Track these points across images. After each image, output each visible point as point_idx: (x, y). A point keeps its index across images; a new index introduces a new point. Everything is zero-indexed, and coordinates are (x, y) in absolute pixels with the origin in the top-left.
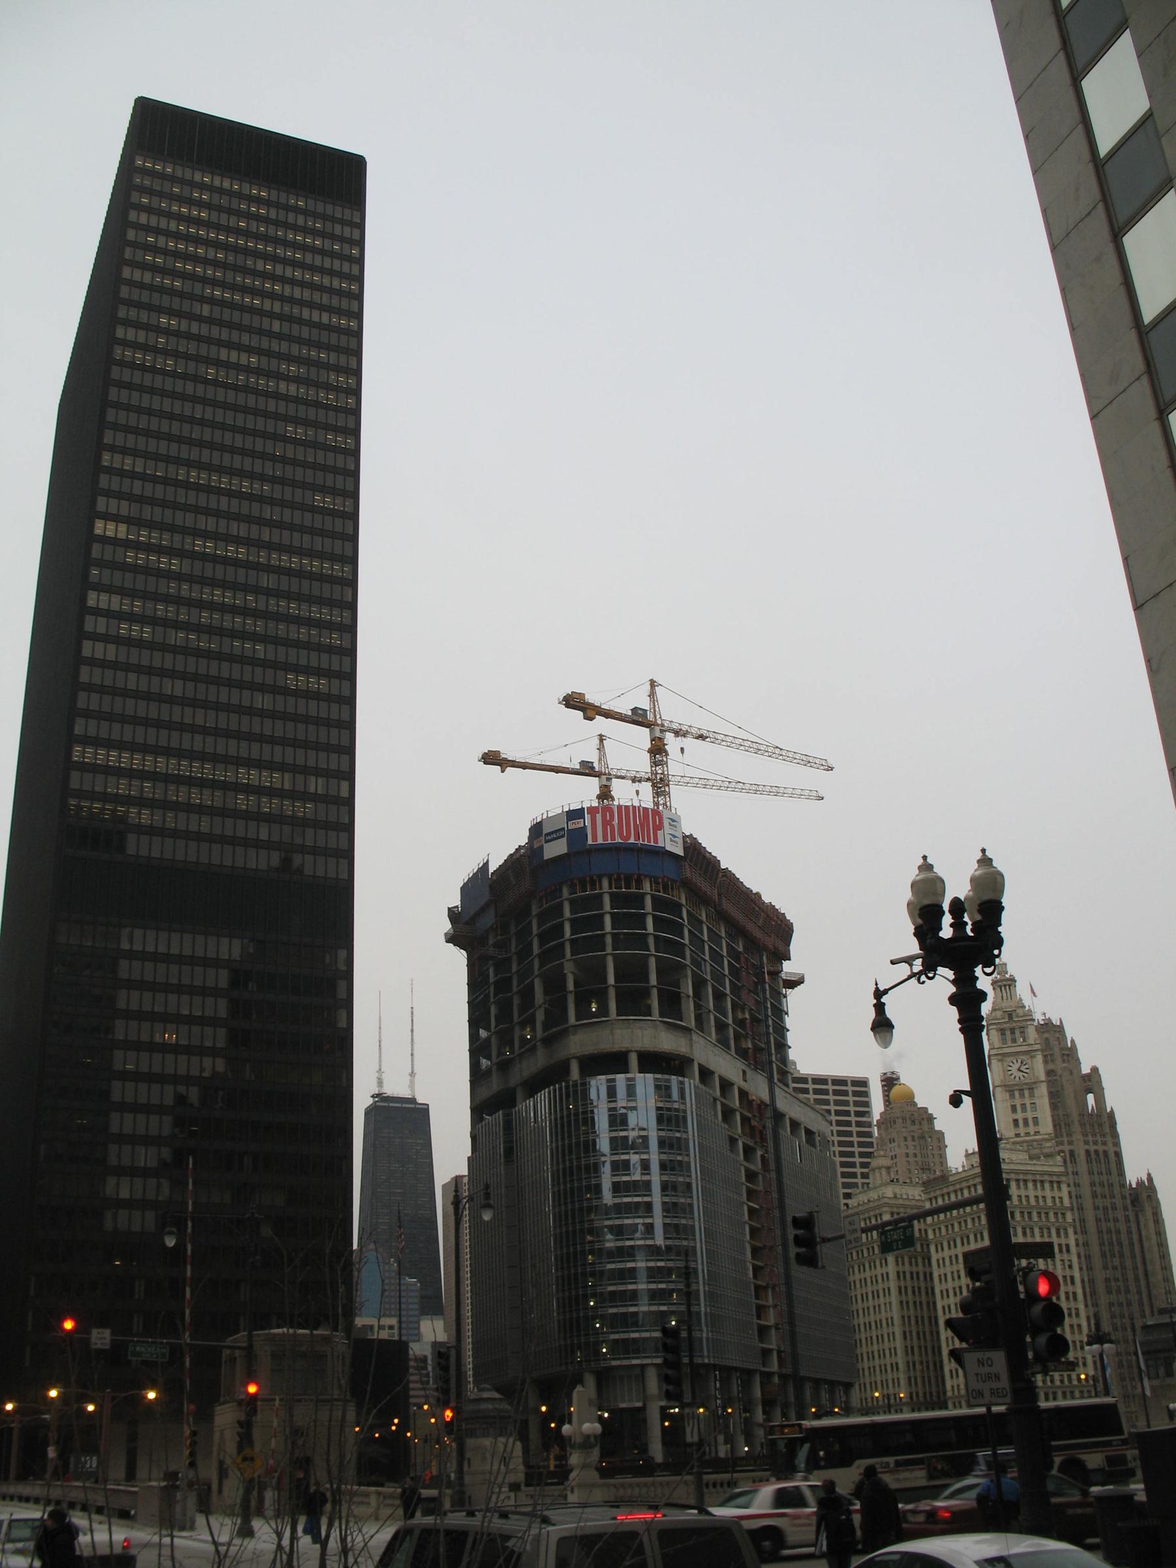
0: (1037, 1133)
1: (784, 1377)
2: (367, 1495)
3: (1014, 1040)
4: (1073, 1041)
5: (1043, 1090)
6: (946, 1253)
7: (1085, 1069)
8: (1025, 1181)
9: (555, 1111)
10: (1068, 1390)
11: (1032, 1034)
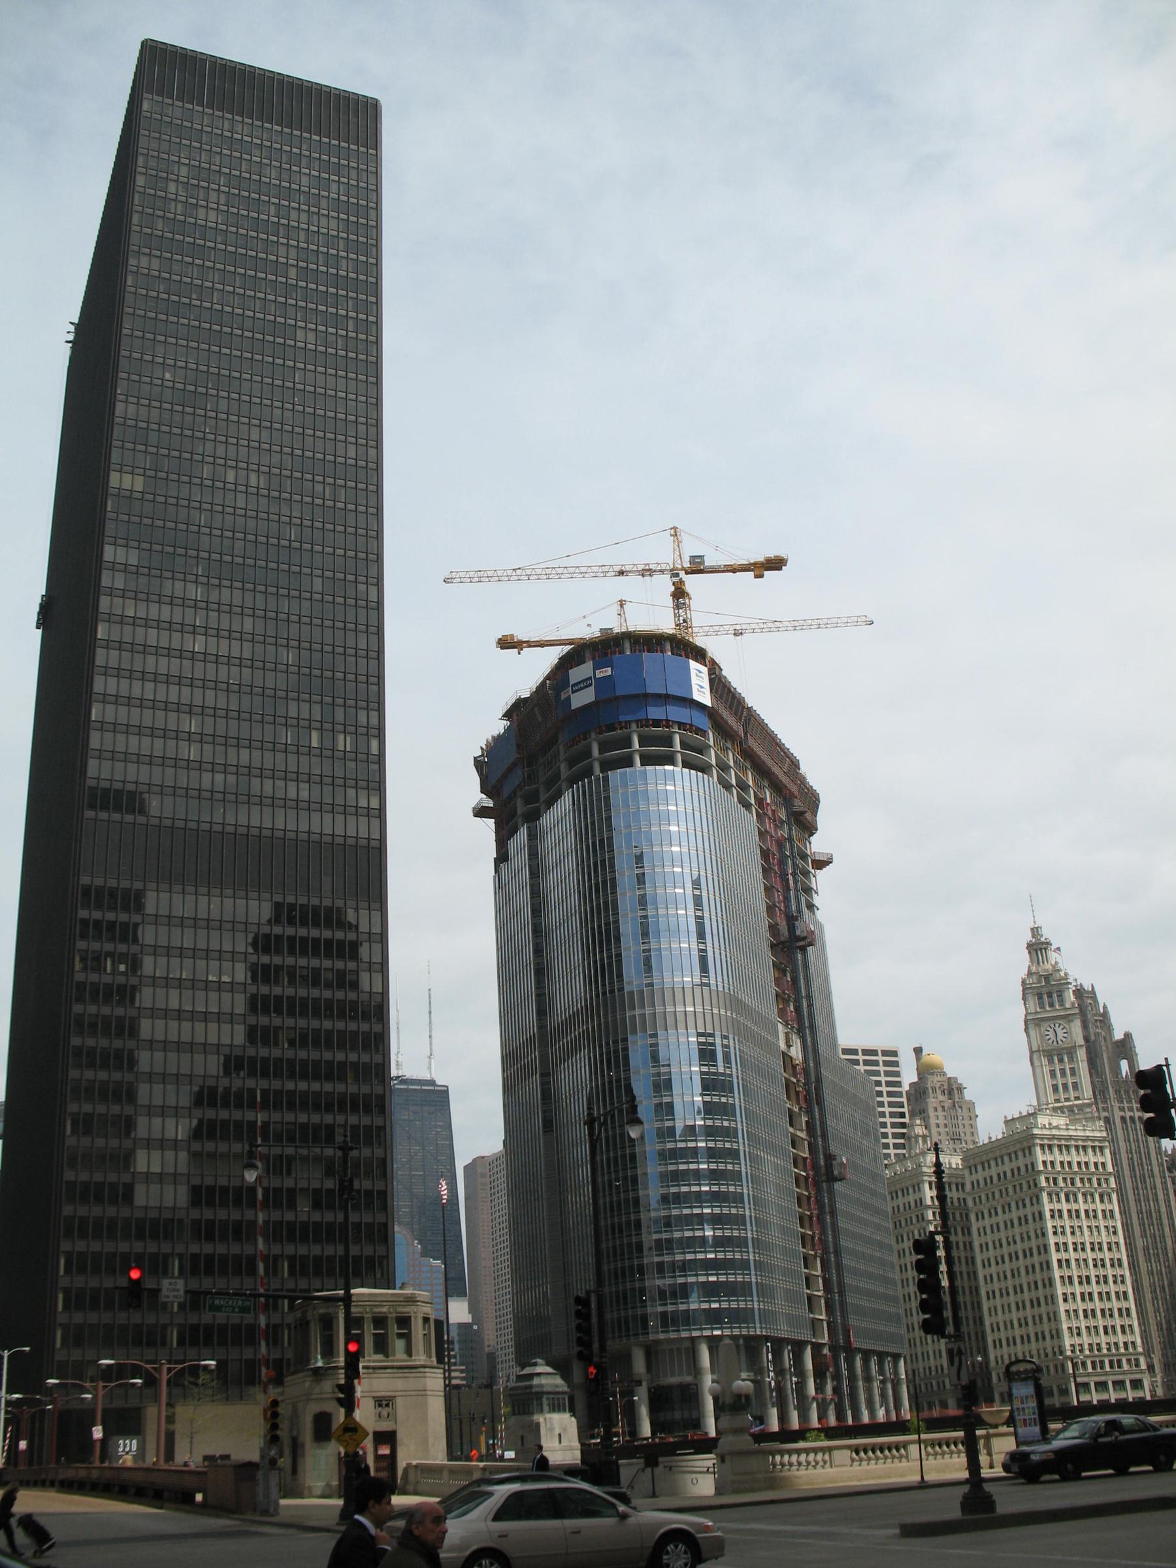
0: (1077, 1098)
1: (834, 1348)
2: (905, 1445)
3: (1051, 1005)
4: (1105, 1007)
5: (1081, 1054)
6: (987, 1222)
7: (1118, 1035)
8: (1067, 1147)
9: (597, 1078)
10: (1115, 1359)
11: (1070, 997)
